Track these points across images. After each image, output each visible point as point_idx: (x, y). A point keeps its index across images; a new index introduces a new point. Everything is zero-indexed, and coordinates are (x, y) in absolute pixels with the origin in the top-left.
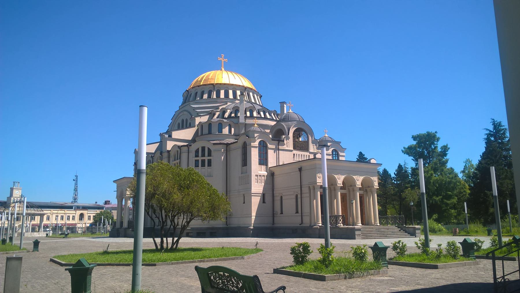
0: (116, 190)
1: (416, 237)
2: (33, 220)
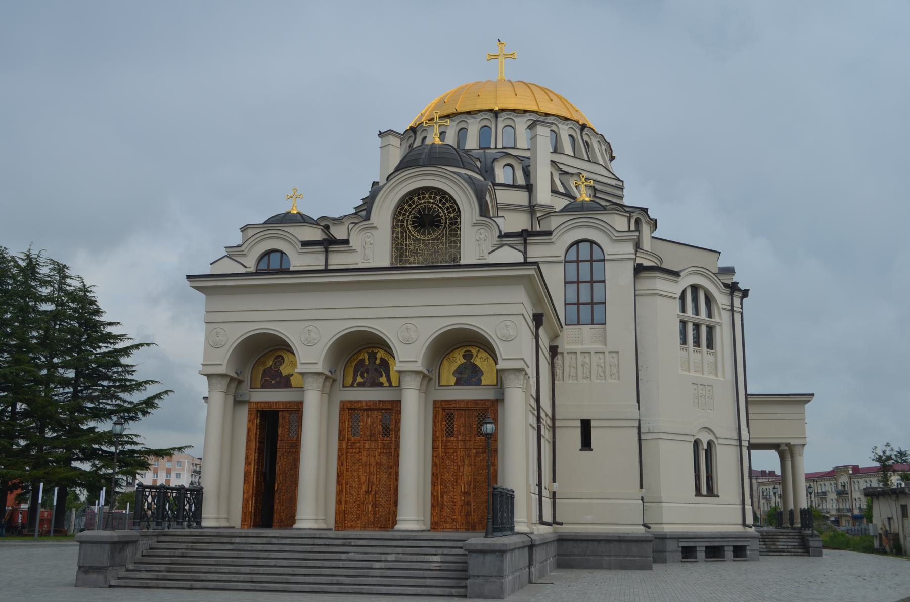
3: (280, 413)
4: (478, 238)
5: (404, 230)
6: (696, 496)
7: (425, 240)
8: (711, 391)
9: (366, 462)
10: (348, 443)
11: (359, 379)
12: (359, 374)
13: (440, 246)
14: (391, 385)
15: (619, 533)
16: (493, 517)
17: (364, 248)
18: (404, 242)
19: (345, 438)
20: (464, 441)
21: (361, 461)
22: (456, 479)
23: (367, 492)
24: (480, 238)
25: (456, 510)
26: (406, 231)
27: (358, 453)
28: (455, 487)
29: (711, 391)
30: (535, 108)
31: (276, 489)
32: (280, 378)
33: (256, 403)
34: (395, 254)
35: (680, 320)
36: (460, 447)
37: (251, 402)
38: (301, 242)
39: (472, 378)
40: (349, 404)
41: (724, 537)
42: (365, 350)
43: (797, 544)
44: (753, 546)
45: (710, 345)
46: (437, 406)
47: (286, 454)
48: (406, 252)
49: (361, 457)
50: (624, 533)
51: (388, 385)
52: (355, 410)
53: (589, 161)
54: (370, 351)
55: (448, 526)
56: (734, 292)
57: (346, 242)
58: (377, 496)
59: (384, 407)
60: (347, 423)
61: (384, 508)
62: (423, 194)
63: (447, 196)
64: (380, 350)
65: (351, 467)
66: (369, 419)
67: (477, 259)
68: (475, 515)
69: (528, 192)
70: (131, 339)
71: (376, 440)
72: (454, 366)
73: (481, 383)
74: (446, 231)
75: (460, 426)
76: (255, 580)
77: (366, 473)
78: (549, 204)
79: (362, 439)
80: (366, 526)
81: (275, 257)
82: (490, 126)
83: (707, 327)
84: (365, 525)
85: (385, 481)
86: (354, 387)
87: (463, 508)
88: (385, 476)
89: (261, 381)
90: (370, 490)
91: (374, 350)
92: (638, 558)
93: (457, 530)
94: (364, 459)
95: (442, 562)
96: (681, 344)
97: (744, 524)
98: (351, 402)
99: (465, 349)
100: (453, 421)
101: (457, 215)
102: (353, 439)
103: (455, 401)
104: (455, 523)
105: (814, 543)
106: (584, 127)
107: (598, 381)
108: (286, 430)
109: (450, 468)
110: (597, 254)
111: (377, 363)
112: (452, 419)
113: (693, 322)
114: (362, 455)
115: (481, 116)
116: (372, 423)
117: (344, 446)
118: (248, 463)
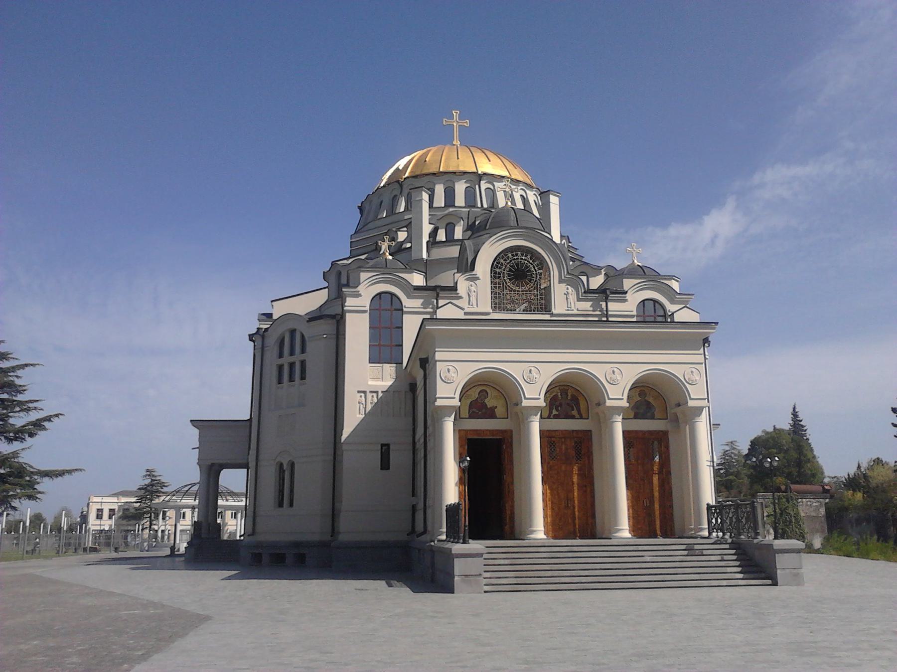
0: (198, 446)
1: (775, 584)
2: (182, 519)
7: (519, 291)
11: (555, 412)
13: (533, 297)
16: (464, 536)
48: (504, 300)
49: (559, 478)
57: (454, 289)
67: (566, 310)
70: (17, 359)
73: (654, 417)
86: (551, 419)
116: (567, 449)
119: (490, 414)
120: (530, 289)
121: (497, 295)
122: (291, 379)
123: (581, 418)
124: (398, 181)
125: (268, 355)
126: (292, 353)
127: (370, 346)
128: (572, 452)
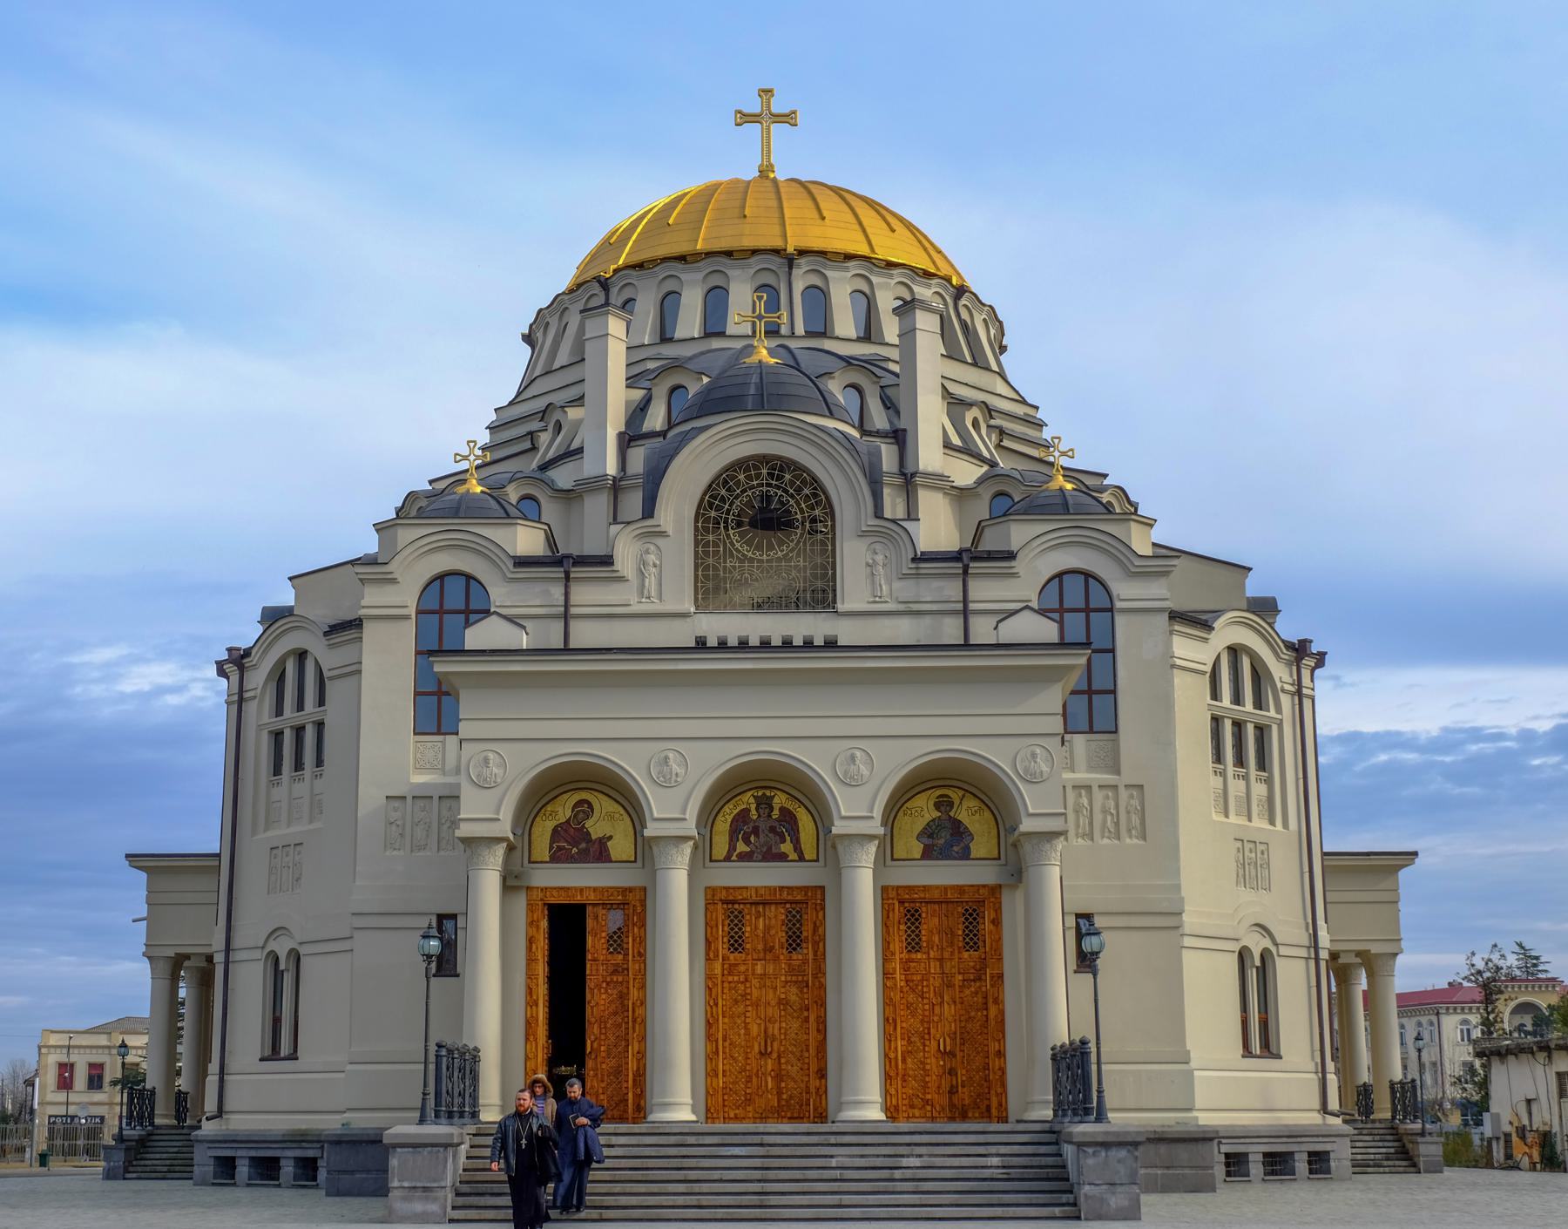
3: (589, 909)
4: (871, 561)
5: (720, 539)
6: (1243, 1057)
8: (1266, 853)
9: (760, 1000)
10: (723, 965)
11: (741, 847)
12: (740, 836)
14: (801, 858)
15: (1152, 1126)
17: (643, 573)
18: (720, 563)
19: (718, 956)
20: (941, 960)
21: (749, 997)
22: (929, 1029)
23: (763, 1054)
24: (874, 560)
25: (929, 1085)
26: (724, 541)
27: (742, 983)
28: (927, 1043)
29: (1266, 853)
30: (863, 249)
31: (589, 1050)
32: (587, 843)
33: (542, 890)
34: (702, 587)
35: (1212, 714)
36: (932, 971)
37: (533, 888)
38: (514, 557)
39: (952, 846)
40: (724, 892)
41: (1294, 1134)
42: (751, 792)
43: (1392, 1150)
44: (1342, 1153)
45: (1262, 764)
46: (891, 896)
47: (604, 985)
49: (748, 991)
50: (1163, 1126)
51: (797, 859)
52: (733, 904)
53: (975, 364)
54: (760, 794)
55: (917, 1112)
56: (1302, 659)
57: (607, 561)
58: (783, 1061)
59: (790, 898)
60: (721, 927)
61: (795, 1082)
62: (756, 468)
63: (805, 475)
64: (778, 793)
65: (730, 1008)
66: (761, 920)
67: (869, 602)
68: (964, 1093)
69: (897, 443)
71: (776, 959)
72: (920, 825)
74: (805, 543)
75: (932, 932)
76: (705, 1204)
77: (761, 1019)
78: (940, 471)
79: (750, 957)
80: (764, 1116)
81: (455, 589)
82: (777, 287)
83: (1255, 727)
84: (762, 1114)
85: (797, 1034)
86: (734, 861)
87: (943, 1082)
88: (795, 1025)
89: (551, 848)
90: (769, 1050)
91: (768, 793)
92: (1187, 1171)
93: (933, 1119)
94: (755, 993)
95: (1004, 1167)
96: (1213, 762)
97: (1324, 1109)
98: (727, 889)
99: (939, 792)
100: (920, 923)
101: (826, 513)
102: (732, 956)
103: (924, 887)
104: (929, 1108)
105: (1429, 1150)
106: (961, 291)
107: (1106, 841)
108: (603, 941)
109: (916, 1009)
110: (1097, 600)
111: (774, 817)
112: (917, 920)
113: (1232, 718)
114: (751, 987)
115: (756, 263)
116: (767, 928)
117: (718, 970)
118: (531, 1003)
119: (599, 852)
120: (787, 554)
121: (711, 573)
122: (298, 765)
123: (801, 858)
124: (598, 279)
125: (251, 709)
126: (300, 706)
127: (416, 694)
128: (781, 936)
